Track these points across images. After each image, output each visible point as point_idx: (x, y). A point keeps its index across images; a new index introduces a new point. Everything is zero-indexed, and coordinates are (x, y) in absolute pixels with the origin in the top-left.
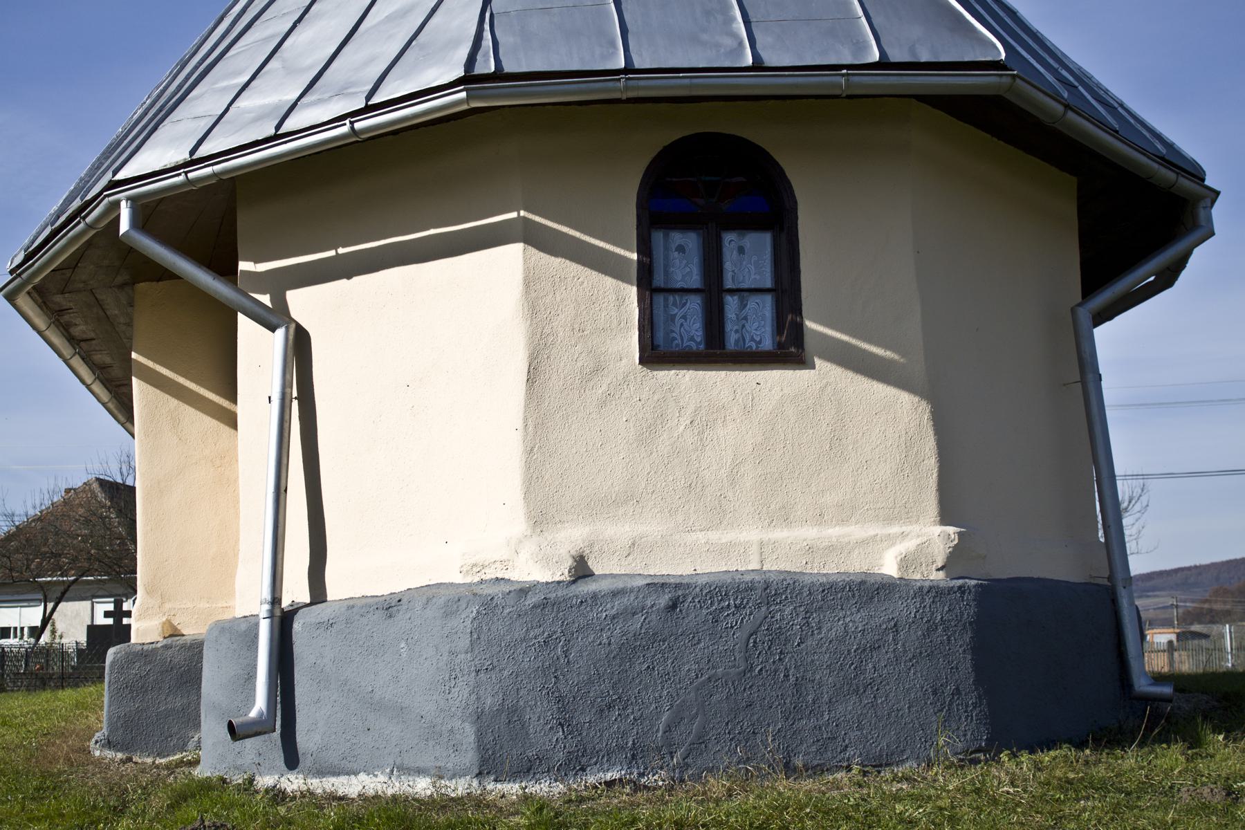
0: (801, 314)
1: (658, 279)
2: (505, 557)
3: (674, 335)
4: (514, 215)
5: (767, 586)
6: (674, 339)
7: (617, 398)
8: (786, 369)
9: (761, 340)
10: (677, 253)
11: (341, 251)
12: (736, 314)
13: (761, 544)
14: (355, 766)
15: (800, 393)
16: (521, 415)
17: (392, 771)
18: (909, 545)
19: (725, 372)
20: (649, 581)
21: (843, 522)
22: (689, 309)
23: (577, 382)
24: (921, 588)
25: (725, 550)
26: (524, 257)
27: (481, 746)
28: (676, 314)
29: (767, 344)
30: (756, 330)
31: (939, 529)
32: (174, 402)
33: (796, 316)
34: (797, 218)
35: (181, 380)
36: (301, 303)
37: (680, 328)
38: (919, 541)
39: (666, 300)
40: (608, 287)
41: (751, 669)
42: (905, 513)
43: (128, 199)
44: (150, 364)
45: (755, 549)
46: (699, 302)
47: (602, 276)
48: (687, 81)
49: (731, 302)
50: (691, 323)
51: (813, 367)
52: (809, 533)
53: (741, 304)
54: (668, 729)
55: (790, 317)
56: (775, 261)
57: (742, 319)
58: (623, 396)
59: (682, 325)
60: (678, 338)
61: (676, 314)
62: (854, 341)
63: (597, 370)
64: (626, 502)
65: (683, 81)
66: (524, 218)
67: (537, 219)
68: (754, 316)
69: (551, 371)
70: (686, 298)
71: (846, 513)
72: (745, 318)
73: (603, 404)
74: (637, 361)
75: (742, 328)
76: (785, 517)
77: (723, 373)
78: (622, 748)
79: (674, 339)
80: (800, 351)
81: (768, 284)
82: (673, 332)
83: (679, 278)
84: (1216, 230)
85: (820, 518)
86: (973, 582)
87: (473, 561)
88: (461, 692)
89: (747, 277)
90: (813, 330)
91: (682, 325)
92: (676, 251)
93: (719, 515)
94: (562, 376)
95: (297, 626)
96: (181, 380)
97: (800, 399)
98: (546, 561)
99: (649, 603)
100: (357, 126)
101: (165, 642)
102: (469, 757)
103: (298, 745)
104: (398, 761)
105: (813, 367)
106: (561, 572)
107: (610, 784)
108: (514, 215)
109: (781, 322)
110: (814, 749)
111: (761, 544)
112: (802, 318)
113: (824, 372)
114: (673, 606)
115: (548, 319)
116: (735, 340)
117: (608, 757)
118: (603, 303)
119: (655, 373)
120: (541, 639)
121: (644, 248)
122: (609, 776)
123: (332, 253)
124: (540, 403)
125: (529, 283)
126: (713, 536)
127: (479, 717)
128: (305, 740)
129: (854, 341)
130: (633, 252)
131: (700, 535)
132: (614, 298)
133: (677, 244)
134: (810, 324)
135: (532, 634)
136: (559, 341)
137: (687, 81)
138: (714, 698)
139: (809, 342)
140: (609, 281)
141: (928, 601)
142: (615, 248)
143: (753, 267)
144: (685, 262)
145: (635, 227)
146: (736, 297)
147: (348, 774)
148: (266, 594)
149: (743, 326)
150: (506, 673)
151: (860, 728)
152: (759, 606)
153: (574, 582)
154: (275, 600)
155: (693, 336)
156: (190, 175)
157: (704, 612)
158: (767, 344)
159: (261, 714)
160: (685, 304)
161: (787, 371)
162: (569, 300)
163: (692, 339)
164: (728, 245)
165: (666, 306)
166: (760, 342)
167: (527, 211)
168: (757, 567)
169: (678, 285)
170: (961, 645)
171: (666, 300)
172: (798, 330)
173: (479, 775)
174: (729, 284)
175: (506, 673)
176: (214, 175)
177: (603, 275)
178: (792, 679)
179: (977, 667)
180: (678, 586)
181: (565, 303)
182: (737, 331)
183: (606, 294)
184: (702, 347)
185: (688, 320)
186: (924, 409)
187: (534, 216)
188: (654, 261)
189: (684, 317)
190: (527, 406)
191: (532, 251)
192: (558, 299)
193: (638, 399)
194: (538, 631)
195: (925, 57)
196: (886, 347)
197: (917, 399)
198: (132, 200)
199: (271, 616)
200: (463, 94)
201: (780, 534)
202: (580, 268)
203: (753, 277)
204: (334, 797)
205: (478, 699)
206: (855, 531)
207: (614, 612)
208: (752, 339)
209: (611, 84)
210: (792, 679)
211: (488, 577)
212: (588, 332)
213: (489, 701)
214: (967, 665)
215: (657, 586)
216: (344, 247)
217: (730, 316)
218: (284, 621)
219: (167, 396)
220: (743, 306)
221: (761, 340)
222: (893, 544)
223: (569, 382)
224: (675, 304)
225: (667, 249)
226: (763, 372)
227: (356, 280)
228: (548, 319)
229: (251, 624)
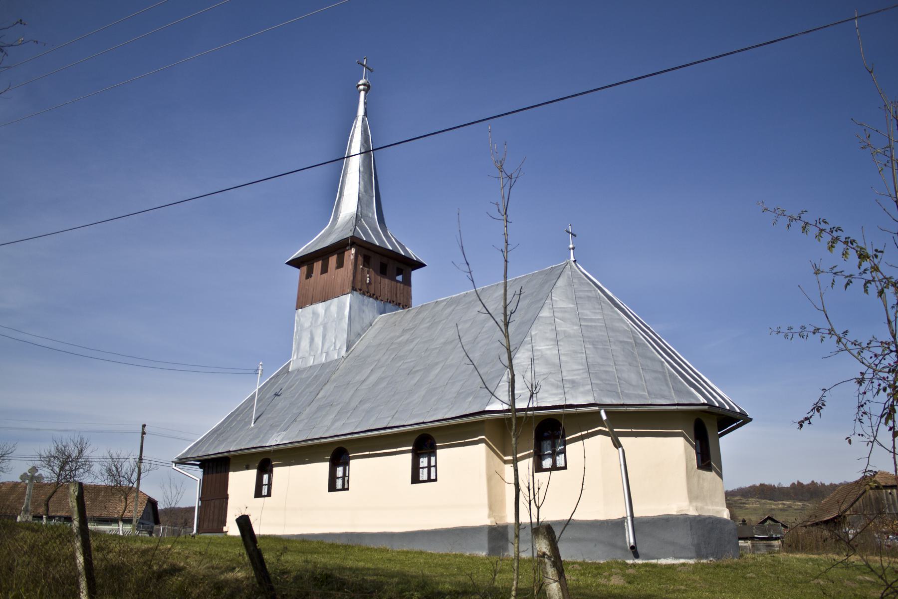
36: (622, 440)
44: (488, 441)
108: (681, 431)
123: (630, 430)
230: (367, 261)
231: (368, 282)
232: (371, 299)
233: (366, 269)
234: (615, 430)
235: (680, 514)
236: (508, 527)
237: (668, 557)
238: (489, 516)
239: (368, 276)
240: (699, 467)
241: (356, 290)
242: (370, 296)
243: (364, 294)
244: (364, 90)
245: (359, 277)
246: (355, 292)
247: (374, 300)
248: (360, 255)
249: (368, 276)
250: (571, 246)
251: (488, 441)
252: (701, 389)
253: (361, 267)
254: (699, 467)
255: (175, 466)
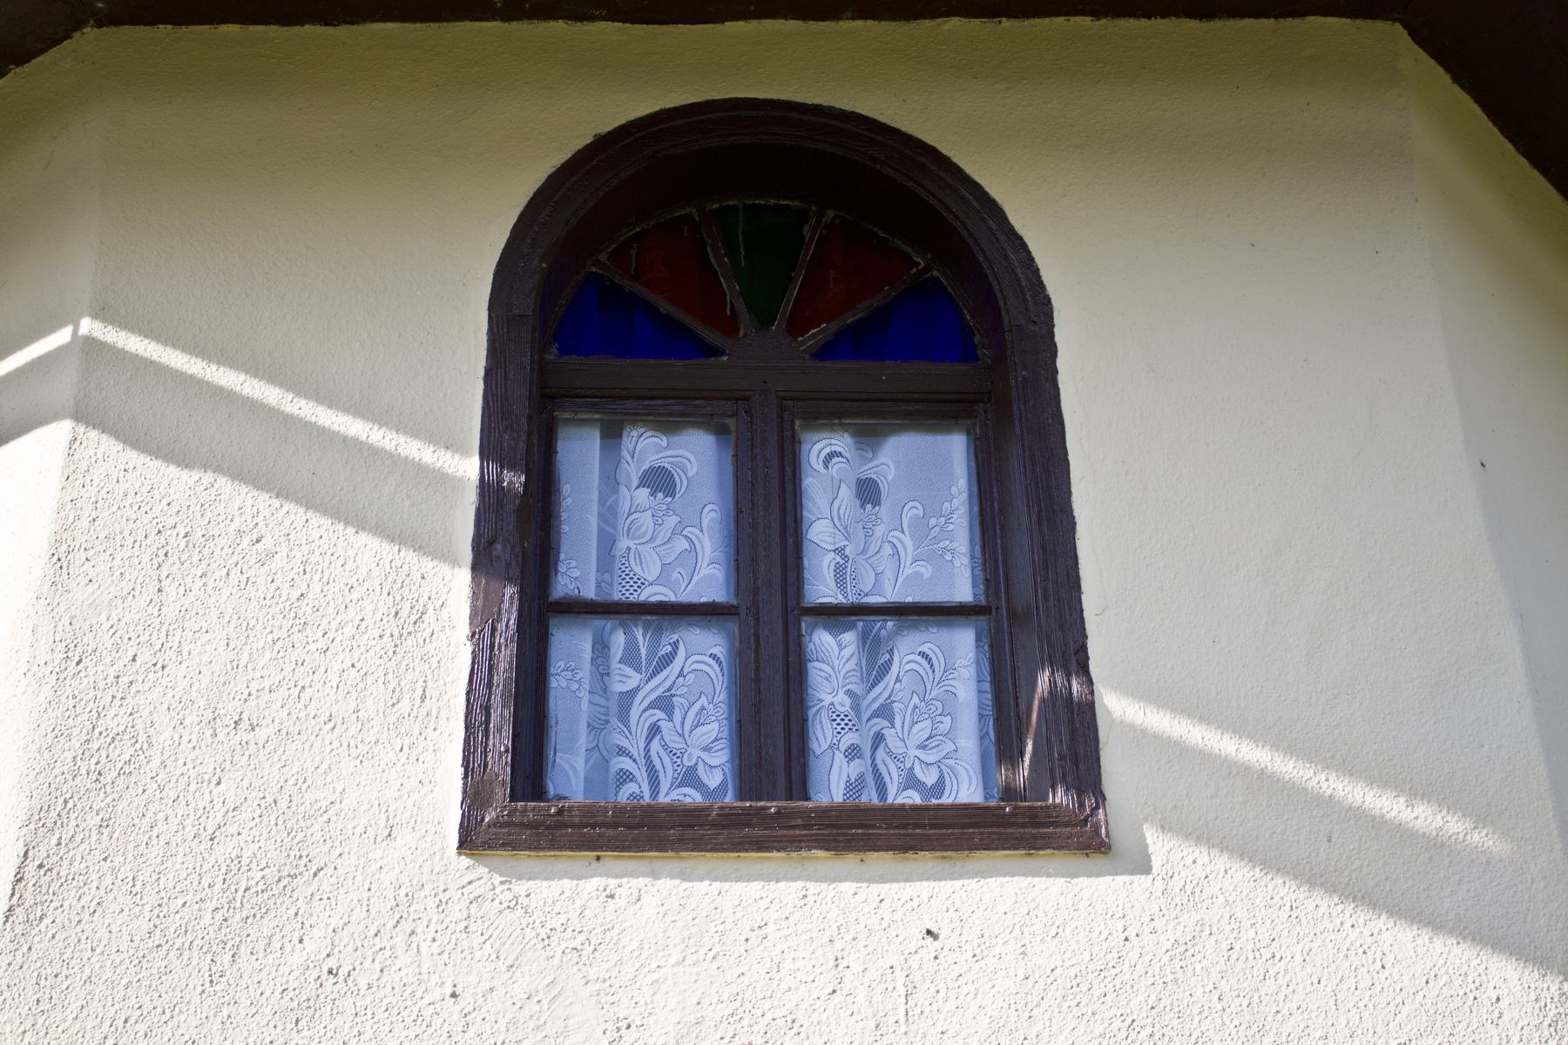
0: (1084, 669)
1: (576, 573)
3: (625, 763)
6: (625, 777)
7: (363, 985)
8: (1033, 875)
9: (941, 780)
10: (645, 492)
12: (849, 693)
15: (1099, 965)
19: (800, 884)
22: (681, 674)
23: (207, 920)
26: (66, 466)
28: (633, 693)
29: (967, 790)
30: (922, 747)
33: (1068, 676)
34: (1053, 351)
37: (649, 739)
39: (601, 647)
40: (363, 572)
46: (716, 650)
50: (687, 727)
51: (1144, 867)
53: (870, 669)
55: (1043, 681)
56: (982, 514)
57: (875, 714)
58: (390, 977)
59: (654, 730)
60: (641, 775)
61: (633, 693)
68: (915, 699)
69: (108, 880)
70: (675, 637)
72: (885, 712)
75: (875, 748)
79: (625, 777)
80: (1089, 803)
81: (963, 590)
82: (622, 752)
83: (652, 572)
89: (889, 575)
90: (1131, 727)
91: (654, 730)
92: (641, 484)
94: (151, 898)
97: (1097, 991)
105: (1144, 867)
112: (1090, 682)
115: (125, 680)
116: (849, 784)
118: (341, 626)
119: (522, 887)
124: (45, 1006)
132: (382, 609)
133: (646, 466)
136: (156, 762)
140: (369, 550)
142: (402, 439)
143: (907, 540)
144: (672, 521)
145: (482, 373)
146: (849, 637)
149: (879, 739)
155: (693, 769)
160: (668, 659)
161: (1041, 882)
162: (214, 615)
163: (690, 778)
164: (820, 467)
165: (602, 671)
166: (939, 787)
167: (104, 320)
169: (653, 594)
171: (601, 647)
174: (822, 588)
177: (351, 530)
181: (191, 624)
182: (853, 753)
183: (355, 595)
184: (729, 799)
185: (677, 716)
187: (123, 334)
188: (564, 516)
189: (664, 703)
191: (99, 444)
192: (170, 611)
193: (448, 990)
203: (908, 571)
208: (911, 782)
212: (271, 730)
217: (828, 699)
220: (875, 668)
221: (941, 780)
223: (174, 922)
224: (630, 659)
225: (611, 482)
226: (947, 886)
228: (125, 680)
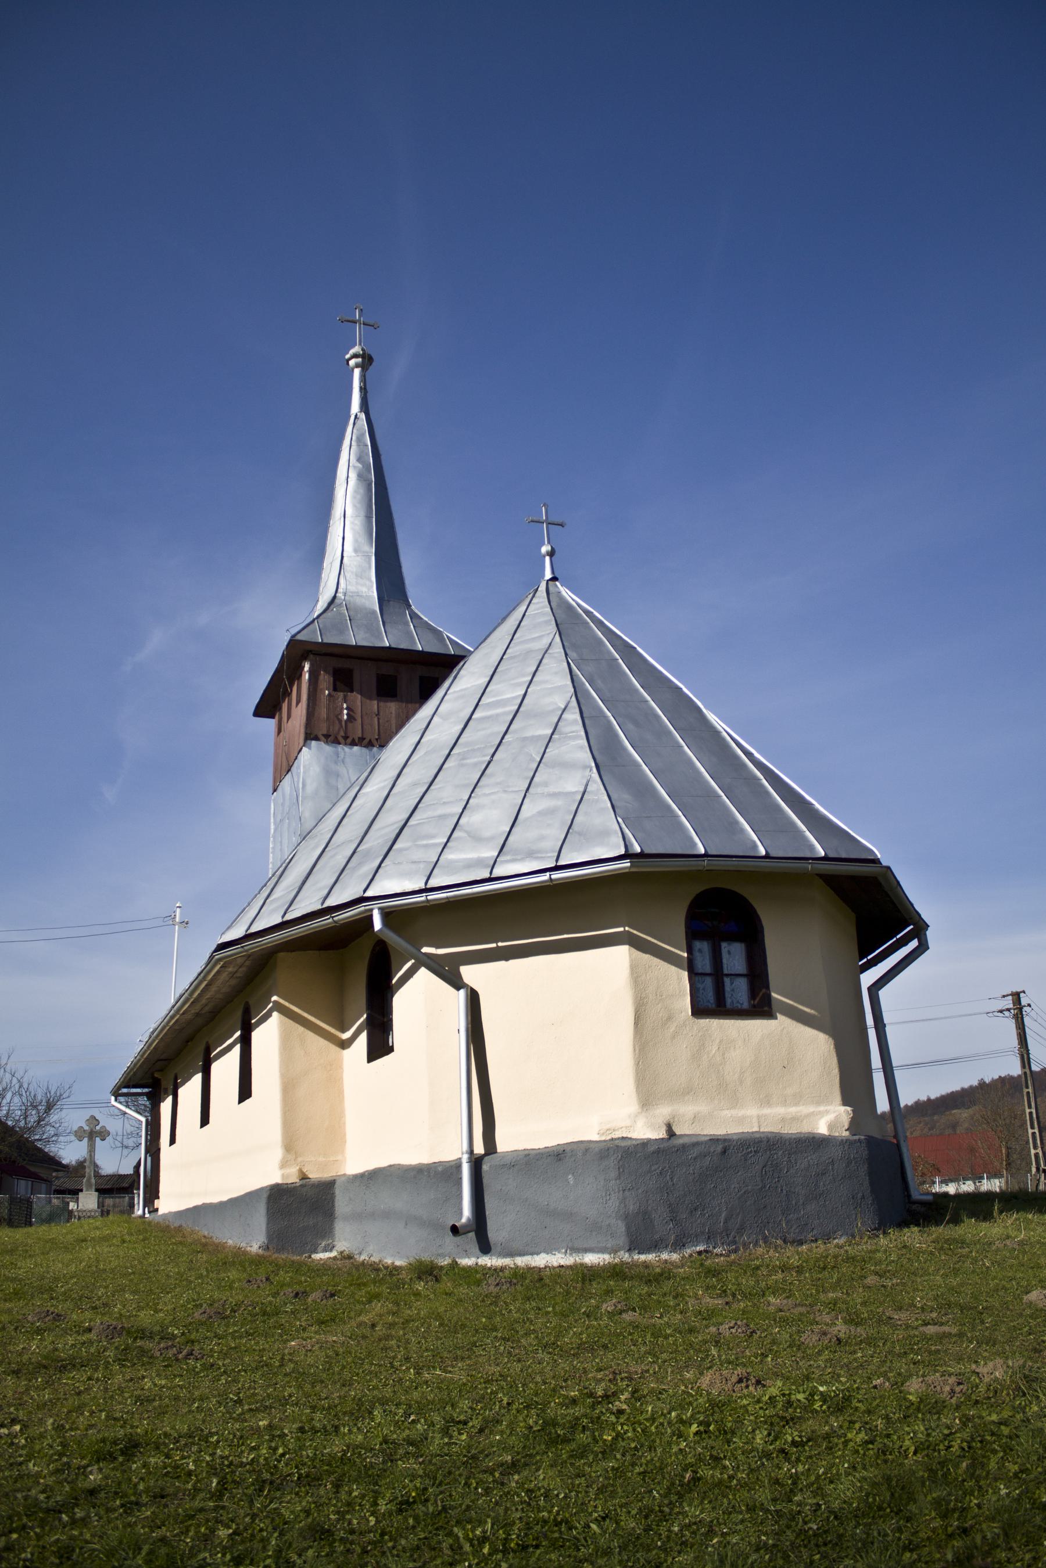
2: (629, 1125)
4: (621, 929)
5: (768, 1140)
11: (500, 944)
13: (759, 1117)
14: (537, 1250)
16: (632, 1043)
17: (566, 1251)
18: (831, 1117)
20: (708, 1138)
21: (796, 1104)
24: (842, 1140)
25: (741, 1120)
27: (629, 1232)
29: (746, 1006)
31: (843, 1108)
32: (301, 1029)
35: (306, 1015)
36: (470, 973)
38: (835, 1115)
41: (765, 1187)
42: (822, 1100)
43: (379, 909)
44: (287, 1004)
45: (755, 1120)
47: (669, 965)
48: (736, 863)
49: (727, 980)
51: (776, 1019)
52: (780, 1111)
54: (726, 1222)
62: (796, 1005)
63: (670, 1018)
64: (688, 1093)
65: (735, 862)
66: (628, 931)
67: (635, 932)
71: (797, 1099)
73: (673, 1037)
74: (690, 1014)
76: (767, 1101)
77: (733, 1021)
78: (703, 1233)
84: (930, 946)
85: (784, 1103)
86: (863, 1137)
87: (608, 1127)
88: (614, 1203)
93: (735, 1101)
95: (485, 1167)
96: (306, 1015)
98: (652, 1127)
99: (712, 1150)
100: (553, 877)
101: (301, 1182)
102: (622, 1240)
103: (490, 1239)
104: (570, 1245)
105: (776, 1019)
106: (661, 1134)
107: (700, 1253)
108: (621, 929)
109: (753, 993)
110: (797, 1231)
111: (759, 1117)
113: (781, 1023)
114: (724, 1151)
117: (696, 1239)
120: (657, 1171)
121: (690, 950)
122: (698, 1249)
123: (494, 945)
125: (634, 967)
126: (734, 1112)
127: (626, 1217)
128: (494, 1234)
129: (796, 1005)
130: (684, 952)
131: (727, 1112)
134: (774, 995)
135: (653, 1168)
137: (736, 863)
138: (748, 1203)
139: (773, 1003)
140: (673, 968)
141: (846, 1148)
147: (532, 1254)
148: (465, 1146)
150: (640, 1191)
151: (819, 1219)
152: (766, 1151)
153: (669, 1139)
154: (471, 1151)
156: (429, 898)
157: (740, 1154)
158: (746, 1006)
159: (469, 1219)
163: (709, 1001)
168: (757, 1130)
169: (700, 971)
170: (863, 1169)
172: (768, 997)
173: (629, 1250)
175: (640, 1191)
176: (447, 898)
178: (784, 1192)
179: (872, 1184)
180: (725, 1140)
186: (831, 1041)
190: (635, 1038)
191: (633, 950)
194: (656, 1167)
195: (844, 856)
196: (812, 1008)
197: (827, 1037)
198: (382, 910)
199: (470, 1161)
200: (629, 864)
201: (766, 1111)
202: (659, 960)
204: (529, 1269)
205: (625, 1206)
206: (804, 1109)
207: (695, 1155)
208: (738, 1002)
209: (700, 863)
210: (784, 1192)
211: (616, 1136)
213: (631, 1208)
214: (867, 1183)
215: (714, 1140)
216: (502, 942)
218: (476, 1163)
219: (297, 1025)
222: (822, 1117)
227: (512, 962)
229: (457, 1166)
230: (343, 681)
231: (345, 717)
232: (356, 748)
233: (341, 695)
234: (912, 927)
235: (608, 1138)
236: (336, 1186)
237: (555, 1250)
238: (283, 1165)
239: (345, 706)
240: (699, 1011)
241: (316, 739)
242: (353, 743)
243: (336, 742)
244: (357, 366)
245: (323, 712)
246: (314, 743)
247: (364, 750)
248: (325, 671)
249: (345, 706)
250: (545, 549)
251: (287, 1004)
252: (678, 816)
253: (327, 692)
254: (699, 1011)
255: (116, 1100)
